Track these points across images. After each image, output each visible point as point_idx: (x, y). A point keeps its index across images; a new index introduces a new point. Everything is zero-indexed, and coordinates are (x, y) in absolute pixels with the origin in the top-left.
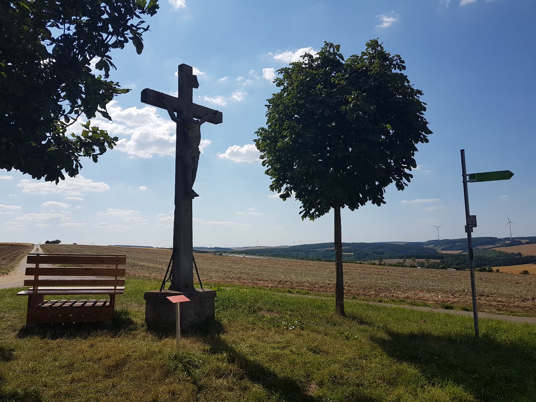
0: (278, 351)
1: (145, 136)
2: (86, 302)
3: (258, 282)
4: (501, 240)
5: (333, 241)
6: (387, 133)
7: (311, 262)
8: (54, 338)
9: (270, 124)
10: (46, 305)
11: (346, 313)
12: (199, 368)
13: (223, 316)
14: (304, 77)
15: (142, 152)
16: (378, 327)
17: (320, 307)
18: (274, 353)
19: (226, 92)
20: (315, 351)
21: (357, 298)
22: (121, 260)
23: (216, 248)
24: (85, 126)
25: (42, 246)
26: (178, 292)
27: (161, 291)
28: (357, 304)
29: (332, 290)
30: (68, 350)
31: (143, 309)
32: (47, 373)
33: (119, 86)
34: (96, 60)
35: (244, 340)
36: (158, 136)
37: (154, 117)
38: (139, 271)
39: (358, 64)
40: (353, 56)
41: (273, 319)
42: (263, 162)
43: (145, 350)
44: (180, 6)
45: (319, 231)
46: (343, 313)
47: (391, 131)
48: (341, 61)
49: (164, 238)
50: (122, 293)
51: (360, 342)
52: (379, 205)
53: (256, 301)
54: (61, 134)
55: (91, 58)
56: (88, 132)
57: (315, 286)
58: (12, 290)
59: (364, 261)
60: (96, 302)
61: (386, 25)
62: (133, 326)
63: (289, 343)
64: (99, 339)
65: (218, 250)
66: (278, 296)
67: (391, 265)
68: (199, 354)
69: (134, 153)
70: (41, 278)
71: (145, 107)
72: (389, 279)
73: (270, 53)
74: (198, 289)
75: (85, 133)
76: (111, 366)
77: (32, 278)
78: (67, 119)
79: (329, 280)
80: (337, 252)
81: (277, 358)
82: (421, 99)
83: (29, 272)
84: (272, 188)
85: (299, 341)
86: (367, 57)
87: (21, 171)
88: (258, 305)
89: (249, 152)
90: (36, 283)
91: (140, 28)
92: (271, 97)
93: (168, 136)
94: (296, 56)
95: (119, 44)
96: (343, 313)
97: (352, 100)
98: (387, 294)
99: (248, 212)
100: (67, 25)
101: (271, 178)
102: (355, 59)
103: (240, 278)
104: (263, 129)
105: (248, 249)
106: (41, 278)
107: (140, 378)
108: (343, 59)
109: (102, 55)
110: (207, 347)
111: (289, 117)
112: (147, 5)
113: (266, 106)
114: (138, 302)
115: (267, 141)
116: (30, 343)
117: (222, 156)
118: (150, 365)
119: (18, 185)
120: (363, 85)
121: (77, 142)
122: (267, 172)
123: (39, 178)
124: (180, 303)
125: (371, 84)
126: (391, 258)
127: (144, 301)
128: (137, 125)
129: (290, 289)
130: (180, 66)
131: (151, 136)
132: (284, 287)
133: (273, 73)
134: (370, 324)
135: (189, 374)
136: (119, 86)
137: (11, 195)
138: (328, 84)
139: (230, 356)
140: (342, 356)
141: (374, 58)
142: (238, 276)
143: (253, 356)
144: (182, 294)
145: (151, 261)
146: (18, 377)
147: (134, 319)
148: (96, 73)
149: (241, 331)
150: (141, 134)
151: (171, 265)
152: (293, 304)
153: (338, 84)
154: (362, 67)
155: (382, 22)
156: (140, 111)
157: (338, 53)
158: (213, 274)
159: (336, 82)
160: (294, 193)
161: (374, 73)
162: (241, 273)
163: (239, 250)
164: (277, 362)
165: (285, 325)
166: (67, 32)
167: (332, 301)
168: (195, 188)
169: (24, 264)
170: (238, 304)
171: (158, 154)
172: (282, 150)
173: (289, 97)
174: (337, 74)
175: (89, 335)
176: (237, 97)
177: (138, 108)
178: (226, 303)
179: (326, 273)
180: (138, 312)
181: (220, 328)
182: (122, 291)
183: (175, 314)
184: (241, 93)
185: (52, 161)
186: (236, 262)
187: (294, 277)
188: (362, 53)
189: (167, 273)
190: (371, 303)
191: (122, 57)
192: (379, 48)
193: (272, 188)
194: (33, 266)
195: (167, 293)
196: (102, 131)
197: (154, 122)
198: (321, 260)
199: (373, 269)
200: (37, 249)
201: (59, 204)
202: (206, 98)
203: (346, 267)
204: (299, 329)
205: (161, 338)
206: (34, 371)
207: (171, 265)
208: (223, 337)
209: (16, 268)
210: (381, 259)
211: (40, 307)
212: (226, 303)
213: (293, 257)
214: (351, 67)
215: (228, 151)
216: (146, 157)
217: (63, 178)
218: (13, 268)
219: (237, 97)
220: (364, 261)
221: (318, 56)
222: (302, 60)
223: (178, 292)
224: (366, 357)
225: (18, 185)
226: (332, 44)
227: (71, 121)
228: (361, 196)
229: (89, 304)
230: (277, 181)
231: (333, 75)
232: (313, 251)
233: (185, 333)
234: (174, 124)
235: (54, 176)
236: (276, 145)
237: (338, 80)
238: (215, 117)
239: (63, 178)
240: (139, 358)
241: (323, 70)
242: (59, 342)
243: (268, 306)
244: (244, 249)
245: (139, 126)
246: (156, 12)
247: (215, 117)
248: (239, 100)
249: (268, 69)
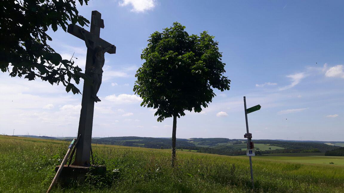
4: (231, 140)
5: (171, 137)
23: (44, 137)
80: (174, 143)
82: (185, 30)
87: (189, 110)
99: (124, 113)
113: (87, 4)
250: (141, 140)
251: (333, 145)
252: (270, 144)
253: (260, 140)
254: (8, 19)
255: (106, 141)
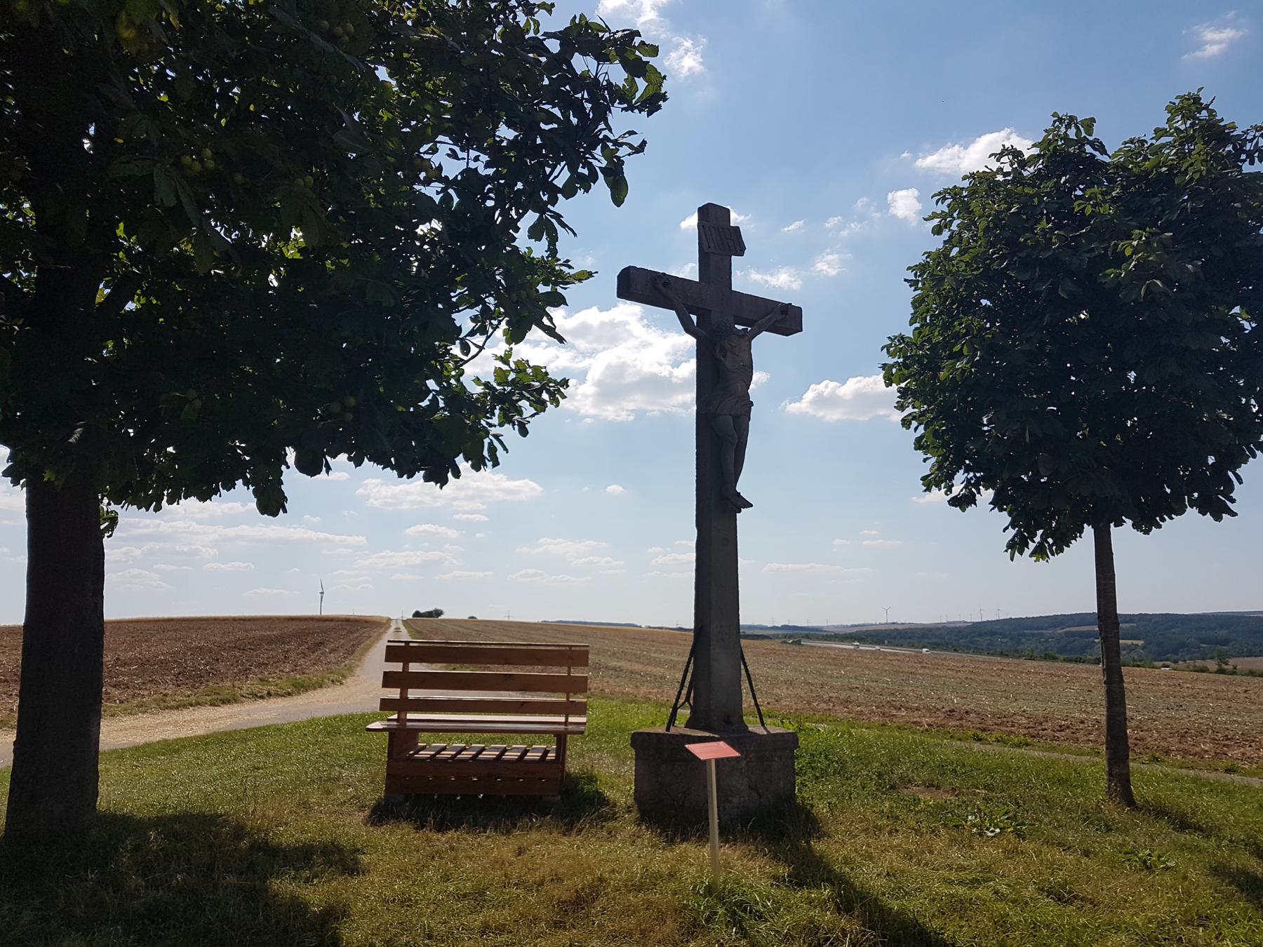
0: (961, 890)
1: (618, 370)
2: (505, 750)
3: (894, 712)
6: (1234, 329)
7: (1030, 663)
8: (441, 828)
9: (918, 325)
10: (424, 754)
11: (1137, 798)
12: (767, 920)
13: (815, 795)
14: (1004, 206)
15: (610, 408)
16: (1230, 841)
17: (1062, 782)
18: (952, 896)
19: (801, 256)
20: (1061, 896)
21: (1163, 761)
22: (577, 657)
23: (785, 627)
24: (502, 359)
25: (406, 622)
26: (707, 734)
27: (668, 729)
28: (1166, 775)
29: (1092, 737)
30: (470, 858)
31: (629, 769)
32: (432, 907)
33: (570, 267)
34: (531, 218)
35: (871, 858)
36: (646, 369)
37: (637, 328)
38: (611, 681)
39: (1146, 159)
40: (1132, 141)
41: (941, 807)
42: (904, 421)
43: (637, 868)
44: (690, 69)
45: (1058, 584)
46: (1128, 799)
47: (1247, 325)
48: (1099, 156)
49: (673, 606)
50: (582, 733)
51: (1185, 878)
52: (1218, 518)
53: (894, 760)
54: (453, 381)
55: (520, 216)
56: (506, 373)
57: (1048, 725)
58: (351, 718)
59: (1176, 662)
60: (525, 752)
61: (1212, 50)
62: (606, 809)
63: (988, 872)
64: (535, 836)
65: (789, 632)
66: (949, 749)
67: (1252, 673)
68: (764, 885)
69: (592, 411)
70: (413, 694)
71: (615, 306)
72: (1250, 711)
73: (905, 155)
74: (754, 727)
75: (499, 373)
76: (563, 902)
77: (394, 693)
78: (465, 348)
79: (1081, 711)
80: (1107, 636)
81: (960, 907)
83: (389, 680)
84: (929, 483)
85: (1014, 869)
86: (1170, 139)
88: (899, 771)
89: (861, 399)
90: (403, 705)
91: (621, 145)
92: (921, 259)
93: (669, 368)
94: (976, 156)
95: (580, 183)
96: (1128, 799)
97: (1135, 253)
98: (1249, 751)
99: (870, 539)
100: (473, 154)
101: (925, 460)
102: (1137, 147)
103: (846, 702)
104: (902, 338)
105: (864, 629)
106: (413, 694)
107: (631, 935)
108: (1104, 152)
109: (541, 208)
110: (784, 871)
111: (969, 306)
112: (638, 95)
114: (615, 753)
115: (918, 371)
116: (397, 838)
117: (793, 407)
118: (649, 905)
119: (360, 491)
120: (1163, 211)
121: (485, 395)
122: (919, 444)
123: (411, 476)
124: (717, 760)
125: (1185, 208)
126: (1251, 654)
127: (631, 753)
128: (600, 347)
129: (979, 732)
130: (700, 210)
131: (631, 371)
132: (962, 726)
133: (915, 201)
134: (1205, 832)
135: (743, 933)
136: (570, 267)
137: (345, 513)
138: (1064, 214)
139: (839, 895)
140: (1136, 914)
141: (1190, 139)
142: (843, 695)
143: (897, 898)
144: (718, 740)
145: (637, 658)
146: (373, 912)
147: (608, 793)
148: (522, 241)
149: (863, 835)
150: (609, 367)
151: (691, 666)
152: (990, 771)
153: (1093, 215)
154: (1158, 166)
155: (1201, 45)
156: (606, 316)
157: (1091, 138)
158: (782, 691)
159: (1088, 211)
160: (987, 495)
161: (1192, 179)
162: (851, 689)
163: (842, 631)
164: (961, 918)
165: (974, 825)
166: (473, 165)
167: (1096, 765)
168: (744, 486)
169: (375, 662)
170: (850, 767)
171: (646, 411)
172: (953, 384)
173: (966, 258)
174: (1089, 192)
175: (515, 826)
176: (827, 266)
177: (601, 310)
178: (821, 763)
179: (1077, 692)
180: (617, 777)
181: (810, 825)
182: (582, 728)
183: (705, 786)
184: (835, 256)
185: (437, 440)
186: (837, 661)
187: (985, 701)
188: (1156, 131)
189: (681, 688)
190: (1204, 774)
191: (585, 210)
192: (1204, 113)
193: (929, 483)
194: (397, 667)
195: (683, 736)
196: (537, 369)
197: (636, 338)
198: (1054, 659)
199: (1203, 683)
200: (397, 630)
201: (442, 529)
202: (755, 276)
203: (1132, 677)
204: (1011, 837)
205: (671, 841)
206: (405, 901)
207: (691, 666)
208: (819, 846)
209: (358, 671)
210: (1222, 658)
211: (411, 759)
212: (821, 763)
213: (979, 651)
214: (1125, 168)
215: (809, 395)
216: (619, 419)
217: (457, 474)
218: (351, 669)
219: (827, 266)
220: (1176, 662)
221: (1036, 151)
222: (994, 166)
223: (707, 734)
224: (1204, 920)
225: (360, 491)
226: (1072, 119)
227: (474, 350)
228: (1168, 491)
229: (511, 755)
230: (940, 466)
231: (1079, 193)
232: (1033, 635)
233: (727, 833)
234: (691, 341)
235: (439, 473)
236: (935, 376)
237: (1094, 206)
238: (785, 319)
239: (457, 474)
240: (626, 886)
241: (1051, 184)
242: (452, 838)
243: (925, 774)
244: (854, 630)
245: (604, 349)
246: (659, 107)
247: (785, 319)
248: (833, 272)
249: (903, 193)
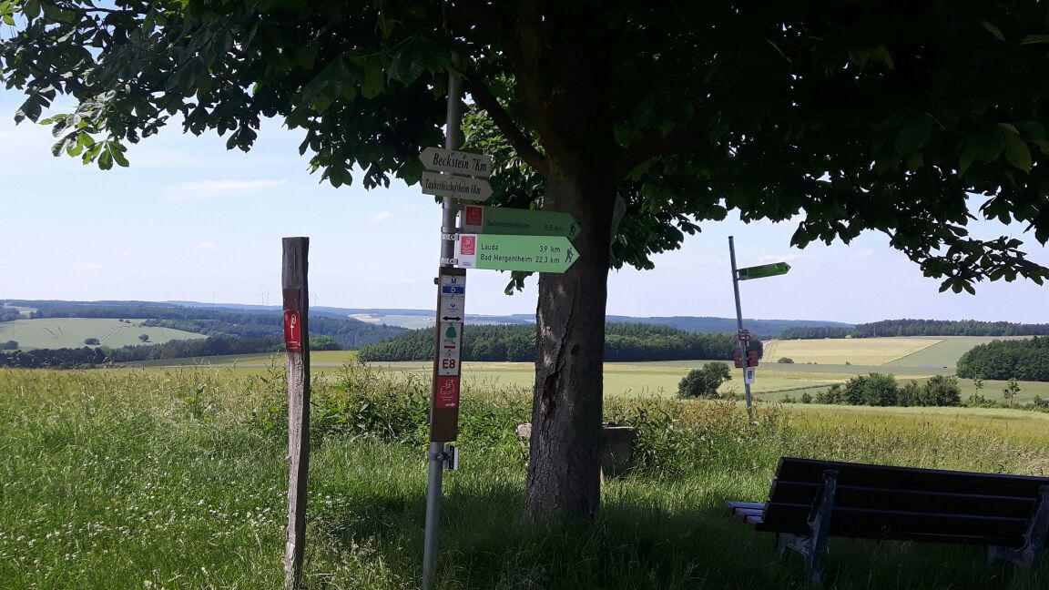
250: (1020, 338)
251: (377, 321)
252: (144, 321)
253: (99, 302)
254: (942, 220)
255: (177, 317)
